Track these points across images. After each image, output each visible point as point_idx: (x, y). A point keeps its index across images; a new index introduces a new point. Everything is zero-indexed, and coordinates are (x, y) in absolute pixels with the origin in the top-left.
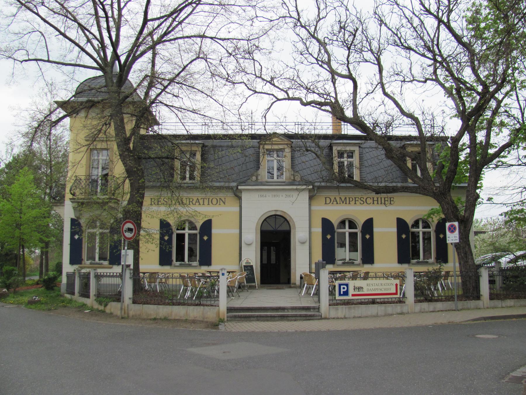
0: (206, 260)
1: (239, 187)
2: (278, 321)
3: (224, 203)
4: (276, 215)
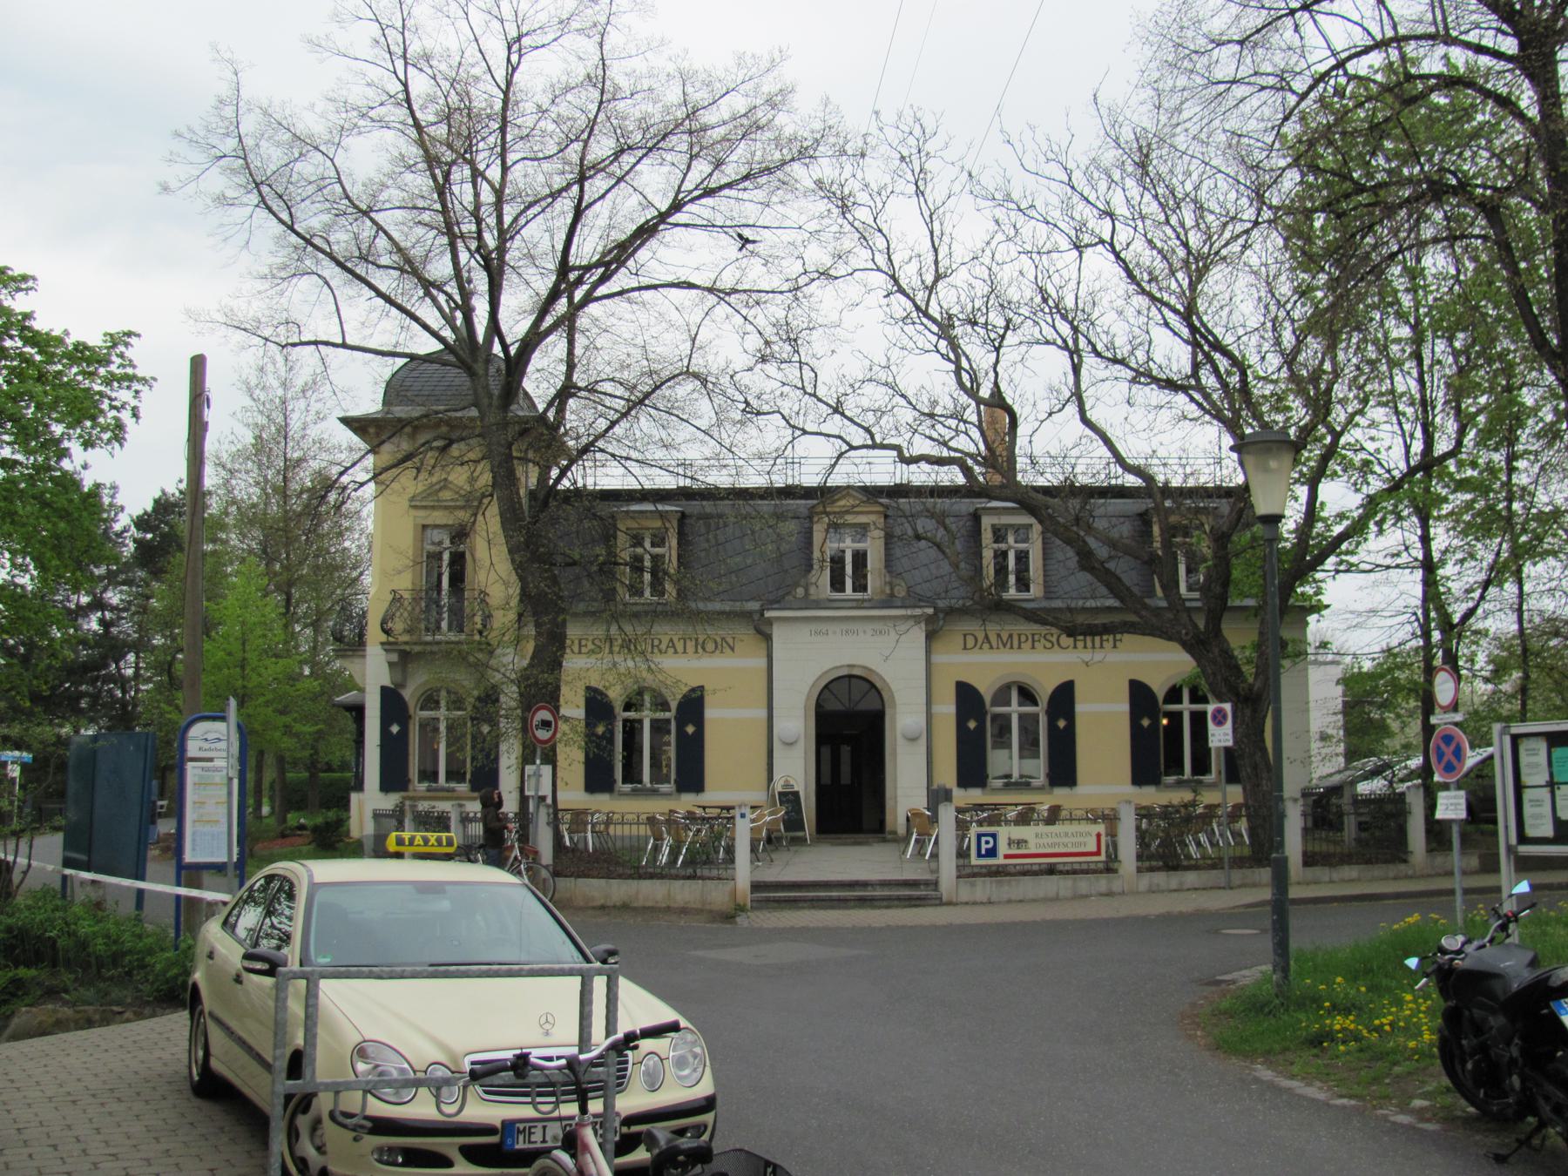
0: (691, 777)
1: (768, 614)
2: (853, 908)
3: (732, 649)
4: (850, 677)
